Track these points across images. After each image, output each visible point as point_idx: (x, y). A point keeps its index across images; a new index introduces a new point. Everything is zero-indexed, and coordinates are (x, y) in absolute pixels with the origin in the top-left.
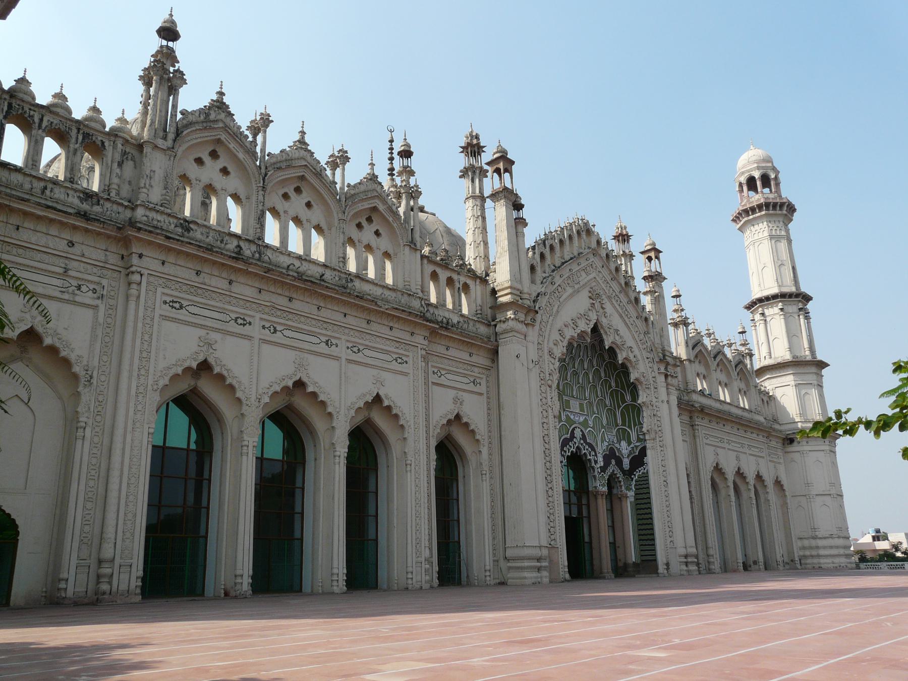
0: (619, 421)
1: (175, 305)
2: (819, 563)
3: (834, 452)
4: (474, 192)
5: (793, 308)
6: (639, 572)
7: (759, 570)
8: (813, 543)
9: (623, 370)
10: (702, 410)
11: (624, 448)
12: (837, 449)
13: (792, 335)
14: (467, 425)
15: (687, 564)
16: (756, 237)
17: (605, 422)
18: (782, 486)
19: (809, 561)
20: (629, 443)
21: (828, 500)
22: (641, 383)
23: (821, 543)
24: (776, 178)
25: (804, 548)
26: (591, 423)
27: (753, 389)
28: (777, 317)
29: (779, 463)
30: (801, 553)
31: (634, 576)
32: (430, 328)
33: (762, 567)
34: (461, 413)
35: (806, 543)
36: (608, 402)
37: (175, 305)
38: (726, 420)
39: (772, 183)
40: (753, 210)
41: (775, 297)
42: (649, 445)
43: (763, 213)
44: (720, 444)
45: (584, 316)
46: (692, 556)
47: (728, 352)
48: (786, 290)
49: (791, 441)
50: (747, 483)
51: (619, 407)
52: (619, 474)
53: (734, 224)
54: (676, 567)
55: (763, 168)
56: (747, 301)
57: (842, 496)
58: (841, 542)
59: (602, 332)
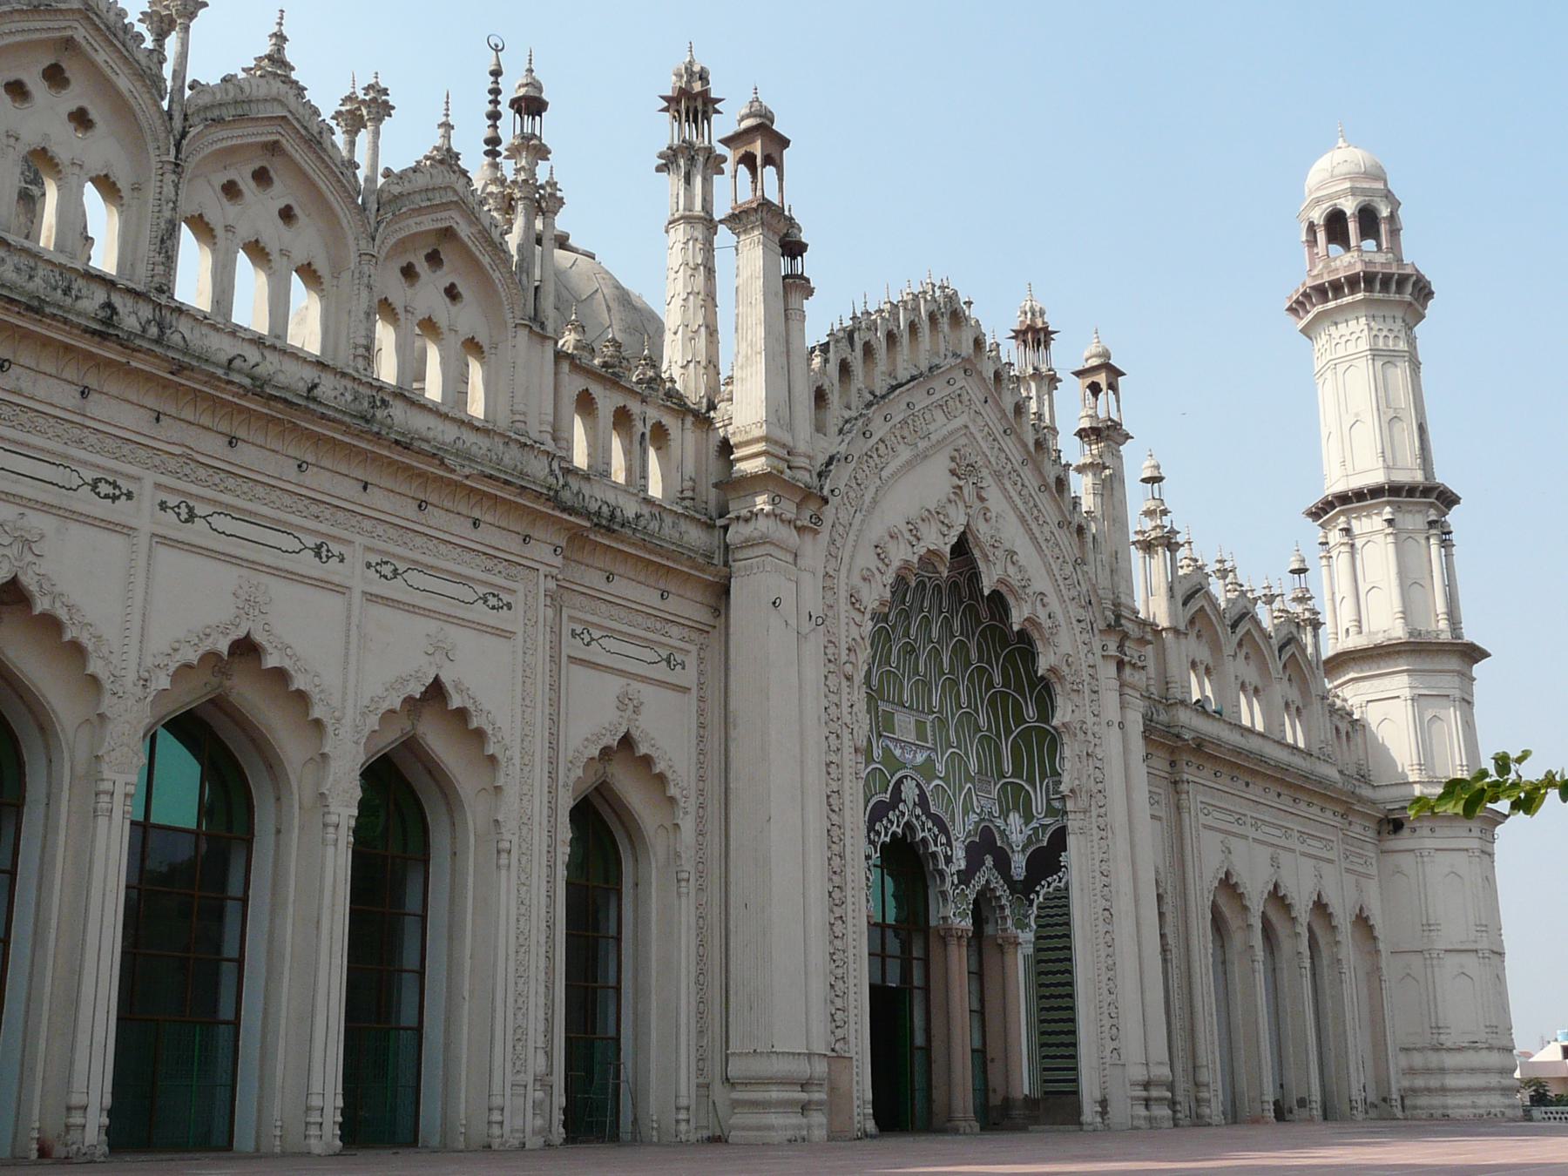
0: (1008, 767)
1: (109, 490)
2: (1445, 1107)
3: (1491, 855)
4: (689, 206)
5: (1414, 521)
6: (1036, 1121)
7: (1311, 1120)
8: (1434, 1059)
9: (1023, 647)
10: (1200, 748)
11: (1015, 830)
12: (1498, 848)
13: (1410, 583)
14: (647, 761)
15: (1147, 1102)
16: (1341, 351)
17: (973, 767)
18: (1371, 928)
19: (1423, 1101)
20: (1028, 817)
21: (1470, 961)
22: (1061, 678)
23: (1450, 1060)
24: (1392, 217)
25: (1411, 1071)
26: (940, 767)
27: (1317, 705)
28: (1379, 538)
29: (1368, 876)
30: (1406, 1083)
31: (1021, 1128)
32: (571, 527)
33: (1317, 1112)
34: (635, 734)
35: (1418, 1060)
36: (982, 721)
37: (109, 490)
38: (1254, 773)
39: (1383, 228)
40: (1337, 288)
41: (1376, 492)
42: (1072, 824)
43: (1360, 296)
44: (1235, 828)
45: (936, 514)
46: (1159, 1084)
47: (1266, 616)
48: (1402, 477)
49: (1397, 826)
50: (1294, 919)
51: (1008, 732)
52: (1002, 891)
53: (1292, 318)
54: (1121, 1111)
55: (1364, 192)
56: (1314, 500)
57: (1501, 954)
58: (1494, 1059)
59: (977, 553)
